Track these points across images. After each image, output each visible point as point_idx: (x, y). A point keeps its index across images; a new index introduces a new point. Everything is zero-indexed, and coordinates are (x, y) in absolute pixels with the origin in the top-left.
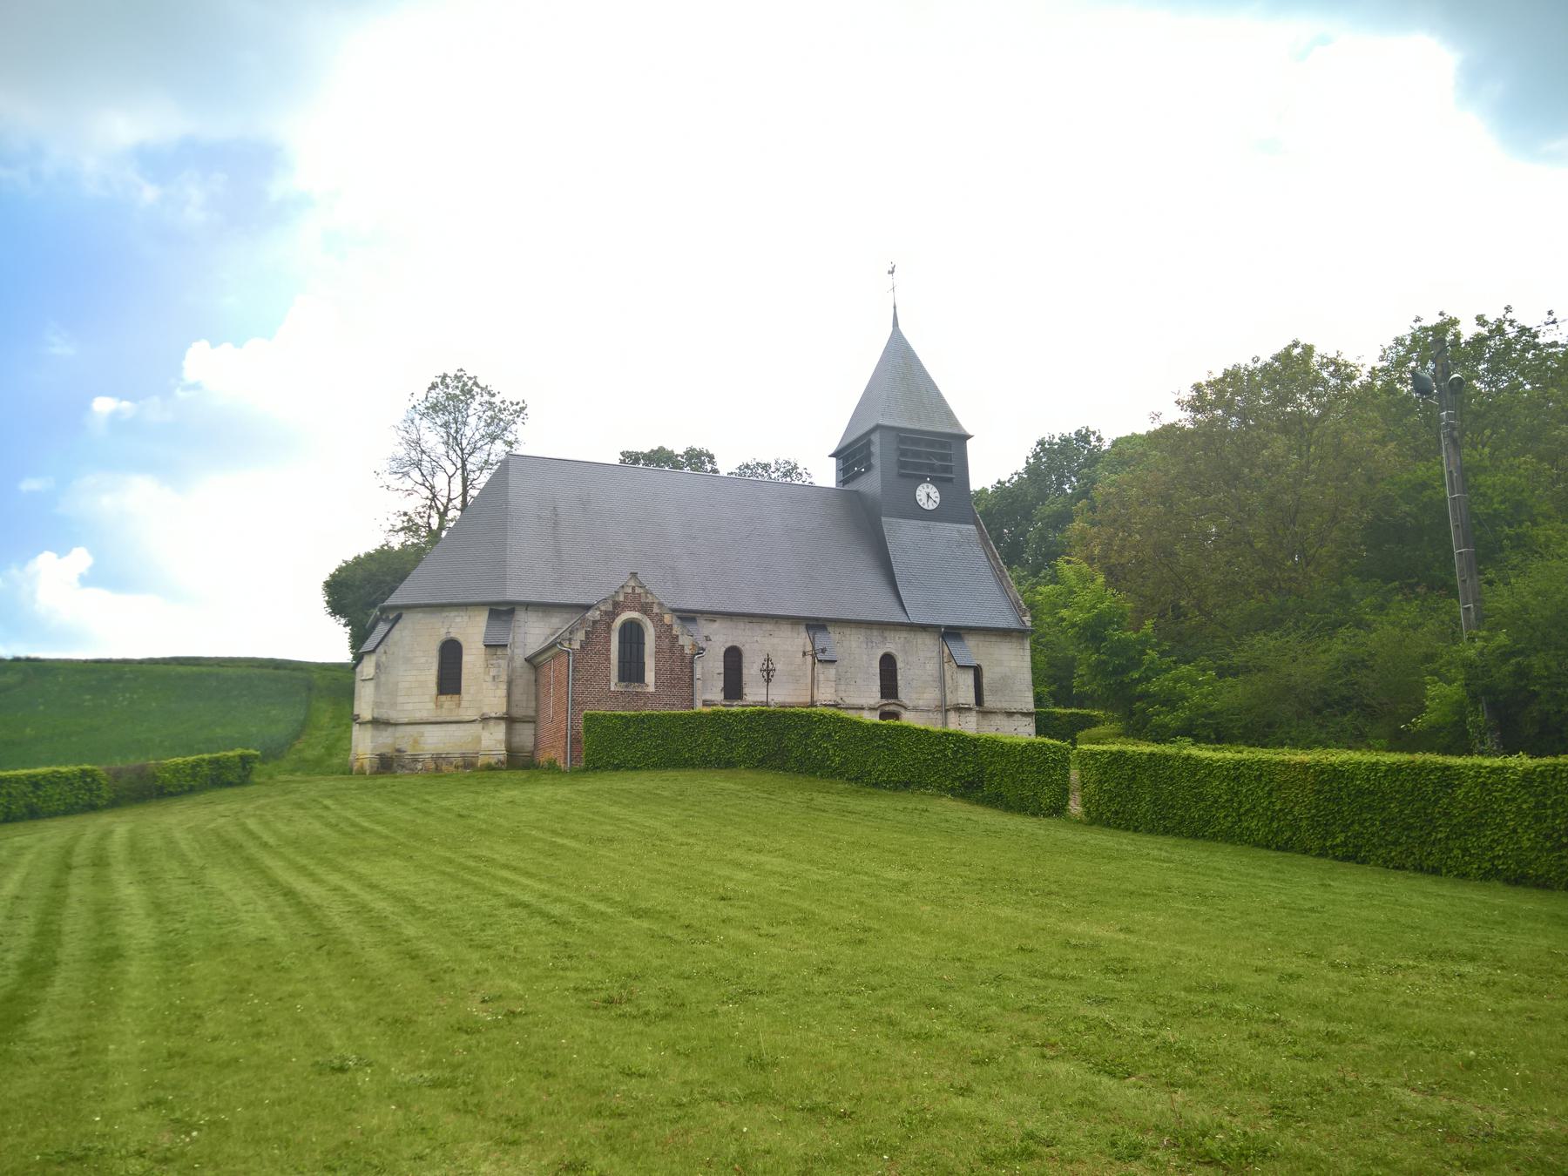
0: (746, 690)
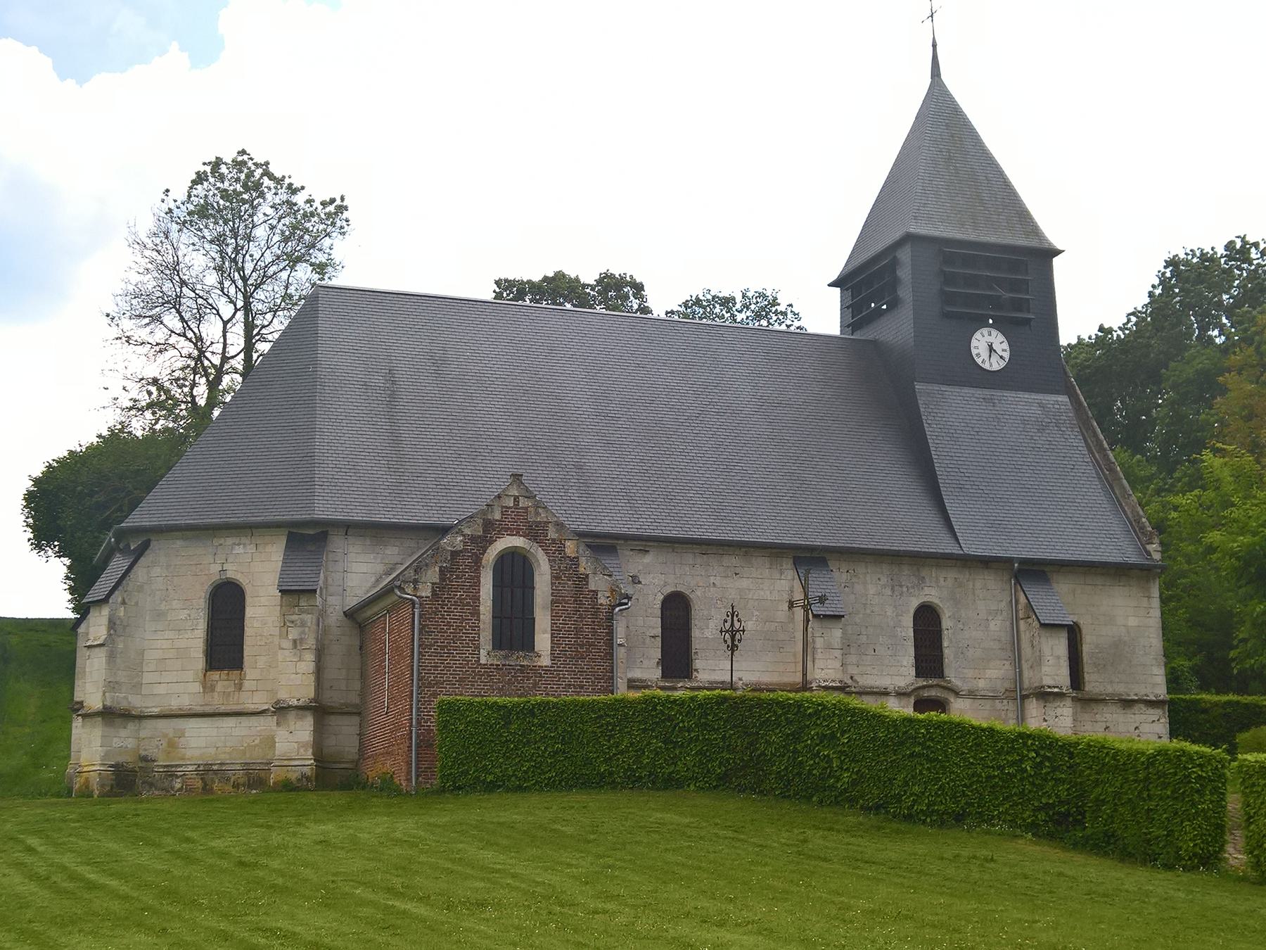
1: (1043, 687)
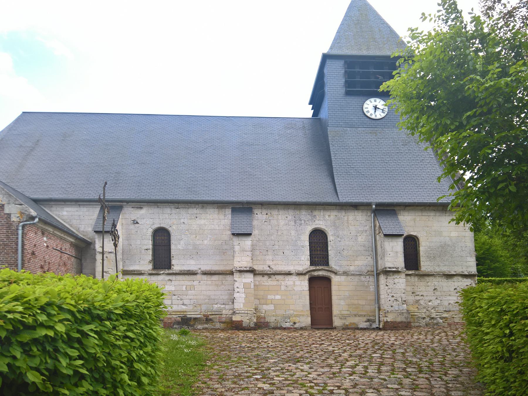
0: (173, 262)
1: (386, 268)
